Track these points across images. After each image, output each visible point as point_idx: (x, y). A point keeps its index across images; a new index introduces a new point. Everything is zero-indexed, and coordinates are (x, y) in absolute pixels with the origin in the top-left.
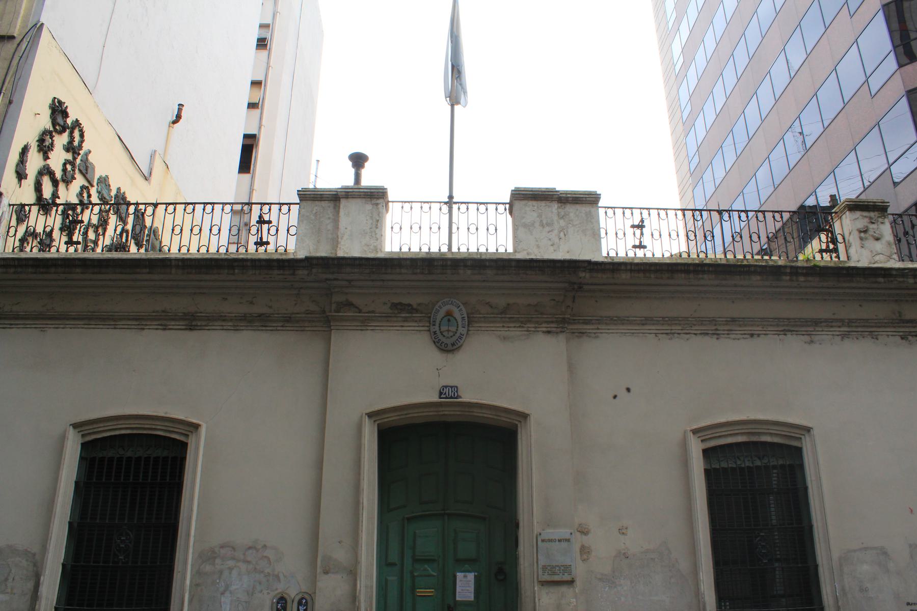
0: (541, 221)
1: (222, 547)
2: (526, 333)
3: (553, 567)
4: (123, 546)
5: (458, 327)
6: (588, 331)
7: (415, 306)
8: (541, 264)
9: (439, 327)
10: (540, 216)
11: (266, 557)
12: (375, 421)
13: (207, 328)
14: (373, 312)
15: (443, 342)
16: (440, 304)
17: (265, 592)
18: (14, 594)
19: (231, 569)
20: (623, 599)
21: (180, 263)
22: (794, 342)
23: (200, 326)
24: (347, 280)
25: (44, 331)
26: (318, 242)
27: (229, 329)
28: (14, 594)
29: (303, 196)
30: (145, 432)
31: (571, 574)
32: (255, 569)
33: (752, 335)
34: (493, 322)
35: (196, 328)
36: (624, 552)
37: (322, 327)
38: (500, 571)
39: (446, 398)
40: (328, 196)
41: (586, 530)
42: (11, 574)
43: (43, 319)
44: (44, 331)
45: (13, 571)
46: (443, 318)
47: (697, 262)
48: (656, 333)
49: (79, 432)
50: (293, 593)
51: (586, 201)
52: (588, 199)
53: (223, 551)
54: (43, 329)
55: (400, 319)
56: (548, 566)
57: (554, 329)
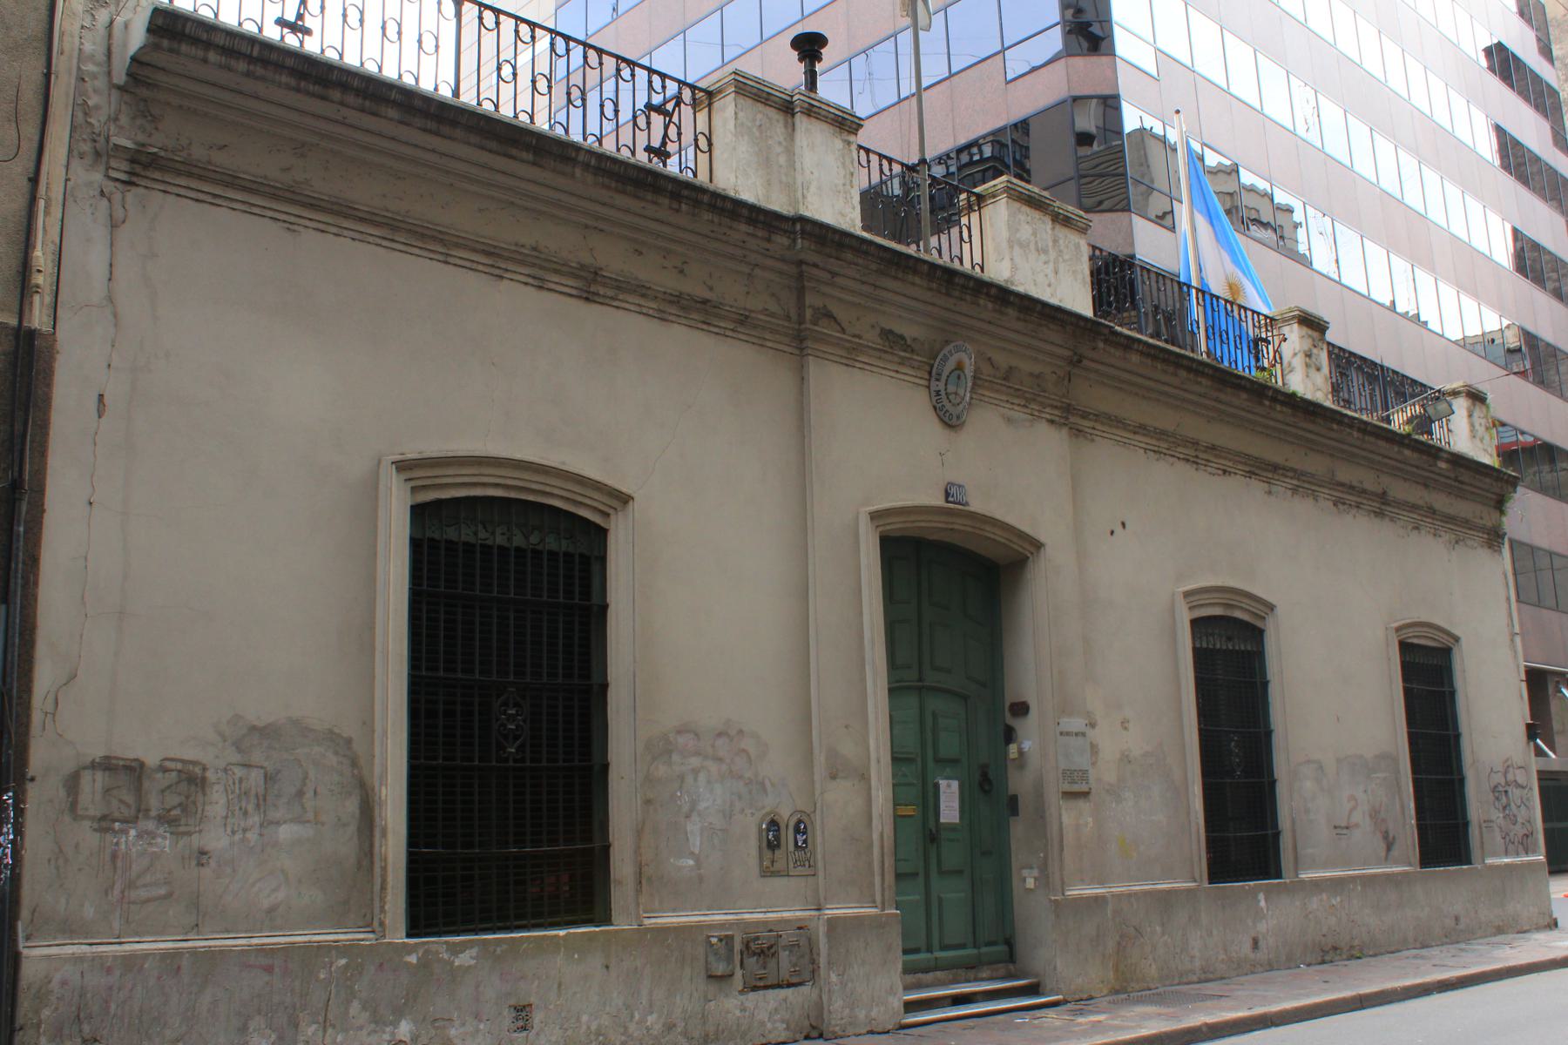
1: (679, 732)
4: (513, 727)
6: (1087, 430)
7: (909, 342)
8: (1122, 340)
9: (946, 385)
10: (1034, 234)
11: (744, 750)
12: (877, 527)
13: (615, 303)
14: (859, 337)
15: (947, 411)
17: (748, 811)
18: (323, 824)
19: (696, 772)
21: (593, 162)
22: (1257, 487)
23: (604, 296)
24: (830, 272)
25: (294, 231)
27: (255, 214)
28: (323, 824)
29: (741, 85)
30: (531, 498)
32: (731, 771)
33: (1225, 472)
34: (997, 391)
35: (596, 298)
37: (789, 345)
40: (777, 99)
42: (307, 781)
43: (190, 175)
44: (294, 231)
45: (312, 774)
46: (953, 371)
48: (1146, 449)
49: (406, 480)
50: (785, 814)
53: (681, 740)
54: (291, 227)
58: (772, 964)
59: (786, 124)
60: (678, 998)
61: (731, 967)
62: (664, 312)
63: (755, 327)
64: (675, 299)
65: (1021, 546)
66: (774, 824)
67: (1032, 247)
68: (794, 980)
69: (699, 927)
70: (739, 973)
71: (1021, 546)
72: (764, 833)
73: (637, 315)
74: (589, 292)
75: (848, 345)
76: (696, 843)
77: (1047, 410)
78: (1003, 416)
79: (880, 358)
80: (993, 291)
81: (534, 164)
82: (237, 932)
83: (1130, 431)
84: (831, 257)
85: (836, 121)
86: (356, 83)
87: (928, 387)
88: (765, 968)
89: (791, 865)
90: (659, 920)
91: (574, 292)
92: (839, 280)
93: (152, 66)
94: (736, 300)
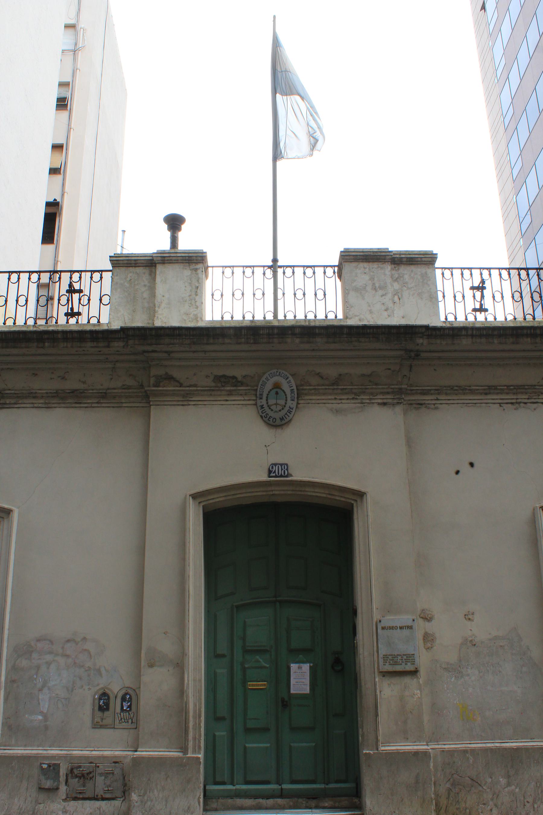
0: (374, 284)
1: (38, 640)
2: (359, 405)
5: (286, 400)
9: (267, 400)
10: (372, 279)
11: (86, 650)
12: (200, 503)
14: (195, 386)
16: (267, 375)
19: (49, 664)
20: (471, 690)
23: (10, 404)
24: (166, 352)
29: (116, 262)
31: (414, 664)
32: (75, 663)
36: (470, 639)
38: (337, 661)
39: (276, 476)
40: (143, 261)
41: (429, 616)
46: (271, 390)
51: (422, 261)
52: (423, 259)
53: (39, 645)
55: (223, 393)
56: (389, 655)
57: (390, 401)
58: (90, 785)
59: (150, 275)
60: (16, 800)
63: (114, 397)
66: (105, 695)
68: (108, 796)
69: (36, 757)
70: (63, 788)
72: (97, 702)
73: (32, 409)
75: (182, 393)
76: (45, 706)
77: (379, 397)
78: (331, 410)
79: (211, 395)
80: (297, 331)
84: (152, 345)
86: (317, 331)
87: (256, 404)
88: (84, 786)
89: (117, 721)
93: (197, 351)
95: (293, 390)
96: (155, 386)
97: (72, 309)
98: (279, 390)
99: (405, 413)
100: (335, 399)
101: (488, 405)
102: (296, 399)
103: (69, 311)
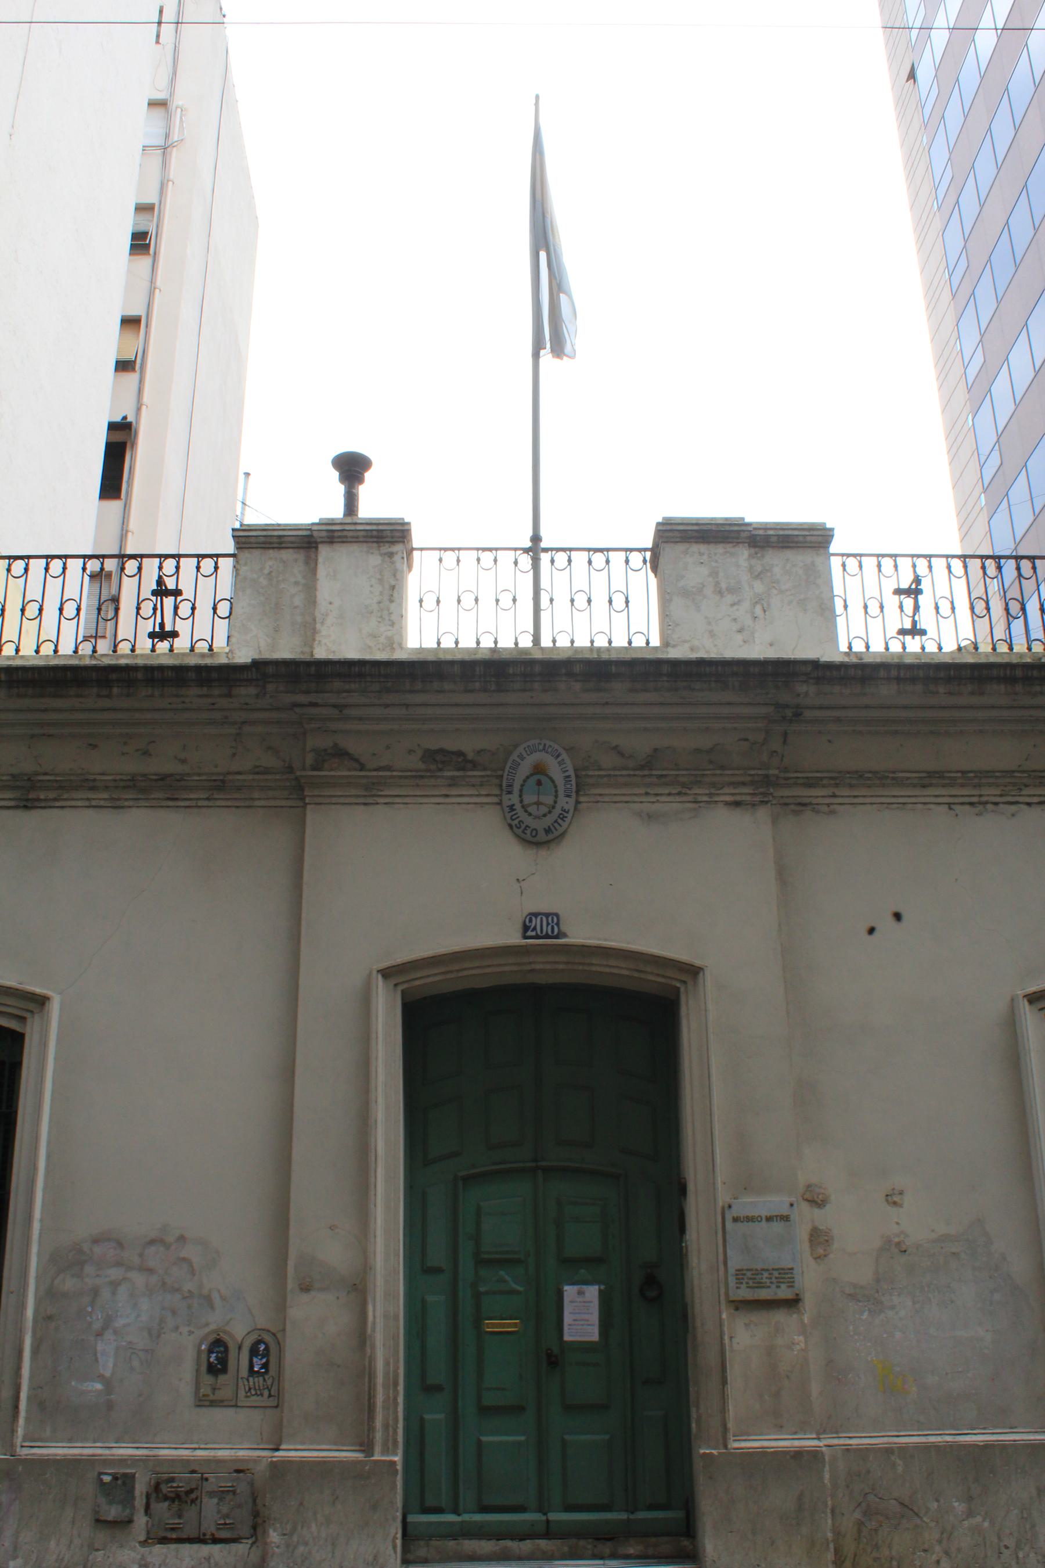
0: (717, 583)
3: (758, 1272)
5: (556, 796)
6: (814, 801)
9: (521, 796)
10: (714, 574)
11: (184, 1259)
12: (396, 985)
13: (57, 804)
17: (185, 1330)
19: (115, 1285)
20: (898, 1335)
23: (45, 800)
24: (334, 706)
26: (276, 630)
29: (243, 540)
31: (792, 1287)
32: (164, 1284)
34: (626, 785)
35: (37, 804)
36: (897, 1240)
39: (537, 937)
40: (293, 539)
46: (528, 777)
47: (1029, 660)
48: (949, 804)
50: (239, 1331)
52: (809, 539)
53: (98, 1250)
56: (748, 1270)
58: (190, 1513)
61: (128, 1511)
62: (119, 799)
63: (239, 789)
64: (131, 783)
65: (664, 976)
66: (219, 1344)
67: (709, 591)
69: (91, 1462)
70: (141, 1520)
71: (664, 976)
72: (204, 1356)
74: (27, 800)
76: (107, 1366)
81: (128, 695)
82: (886, 1431)
83: (914, 786)
85: (372, 537)
88: (180, 1517)
89: (242, 1393)
90: (743, 1444)
91: (12, 803)
92: (346, 712)
94: (216, 766)
95: (569, 777)
96: (314, 769)
97: (162, 625)
98: (543, 779)
99: (775, 820)
100: (647, 794)
101: (928, 806)
102: (574, 795)
103: (157, 629)
